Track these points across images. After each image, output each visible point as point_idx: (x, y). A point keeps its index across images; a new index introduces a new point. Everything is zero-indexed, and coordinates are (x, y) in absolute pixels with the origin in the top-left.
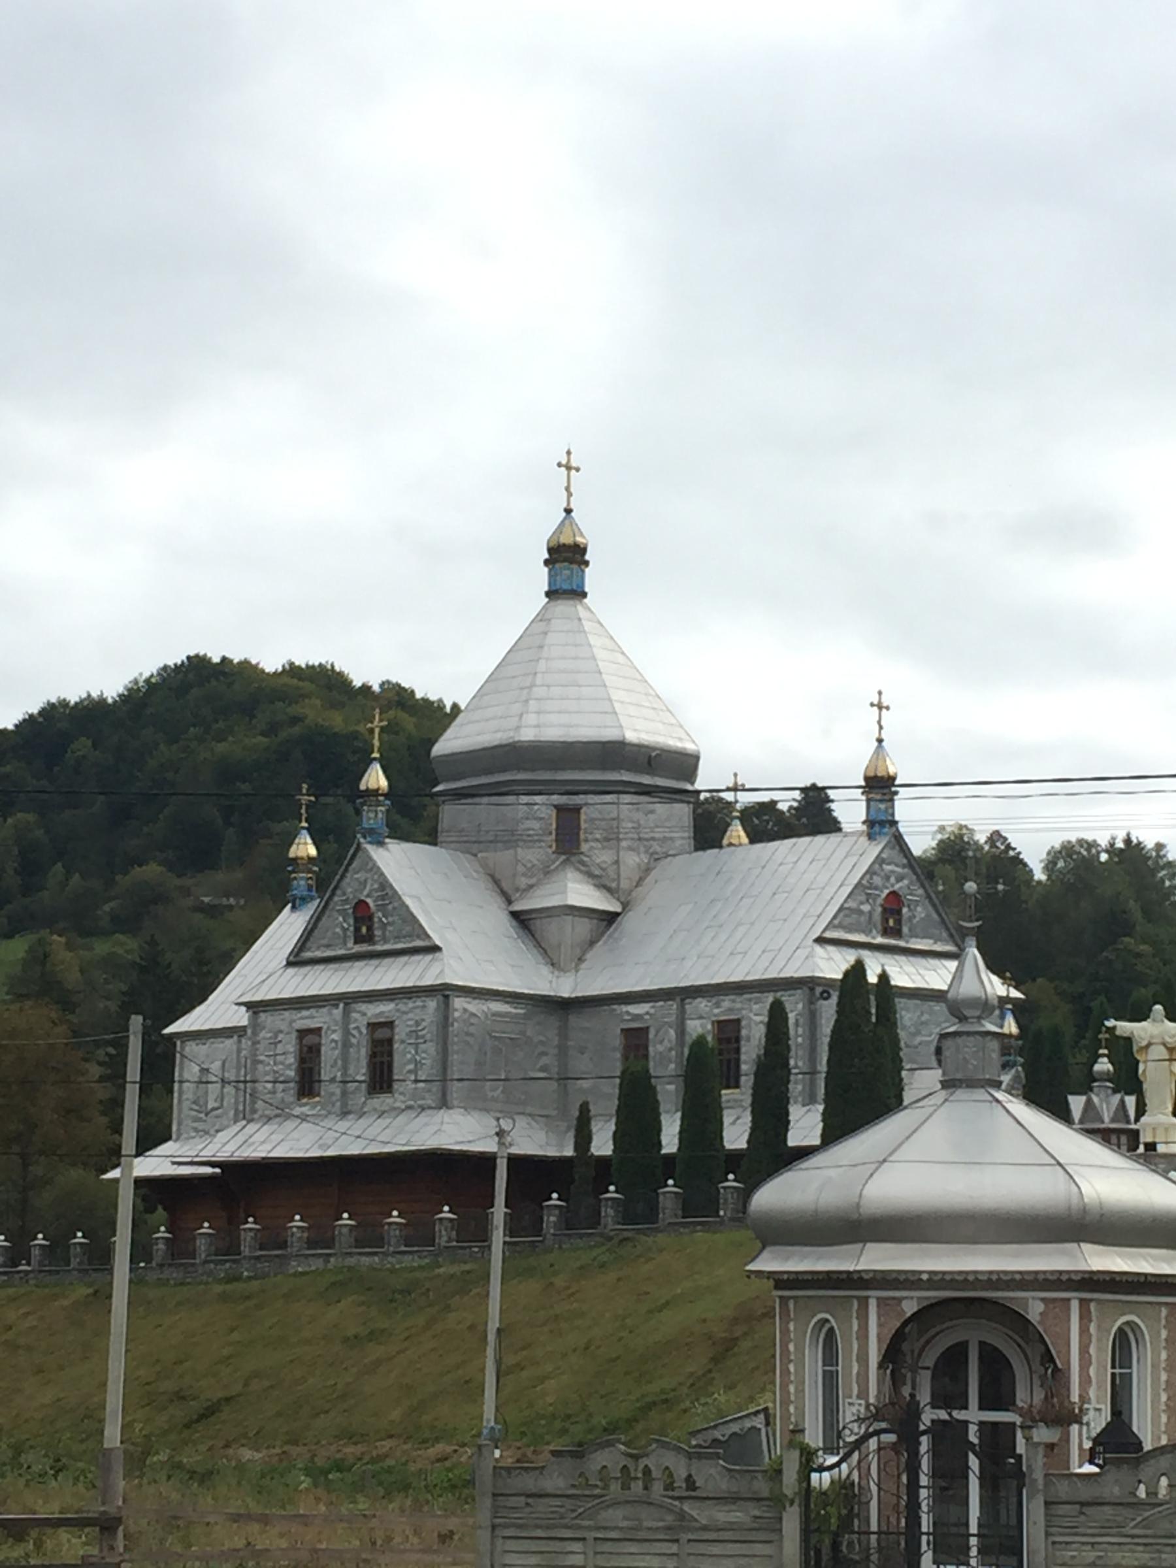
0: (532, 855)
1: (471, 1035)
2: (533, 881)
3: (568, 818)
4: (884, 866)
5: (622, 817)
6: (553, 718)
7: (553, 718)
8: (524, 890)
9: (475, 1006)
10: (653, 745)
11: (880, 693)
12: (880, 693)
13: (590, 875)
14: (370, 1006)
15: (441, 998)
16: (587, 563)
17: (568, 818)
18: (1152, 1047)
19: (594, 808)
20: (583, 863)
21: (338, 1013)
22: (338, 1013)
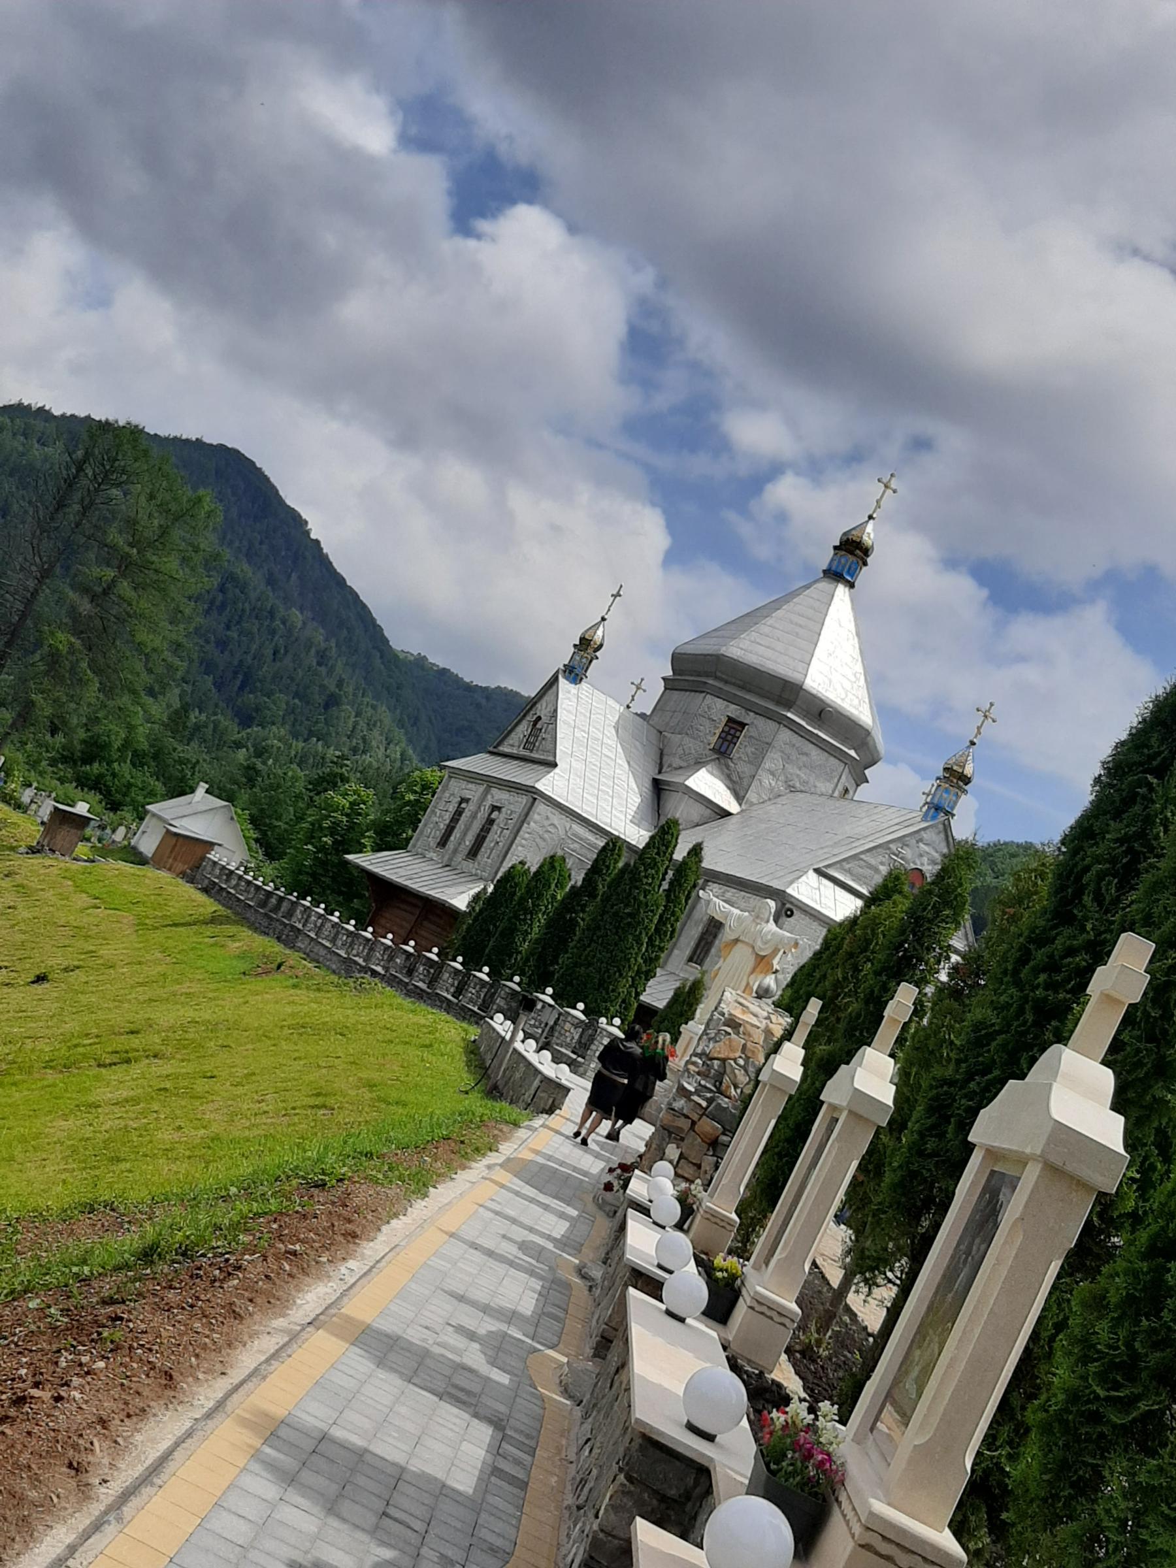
0: (690, 745)
1: (544, 840)
2: (683, 764)
3: (734, 727)
4: (921, 845)
5: (775, 743)
6: (761, 650)
7: (761, 650)
8: (676, 769)
9: (557, 818)
10: (828, 702)
11: (992, 704)
12: (992, 704)
13: (729, 777)
14: (499, 792)
15: (531, 800)
16: (865, 564)
17: (734, 727)
18: (739, 945)
19: (759, 726)
20: (728, 767)
21: (482, 788)
22: (482, 788)
